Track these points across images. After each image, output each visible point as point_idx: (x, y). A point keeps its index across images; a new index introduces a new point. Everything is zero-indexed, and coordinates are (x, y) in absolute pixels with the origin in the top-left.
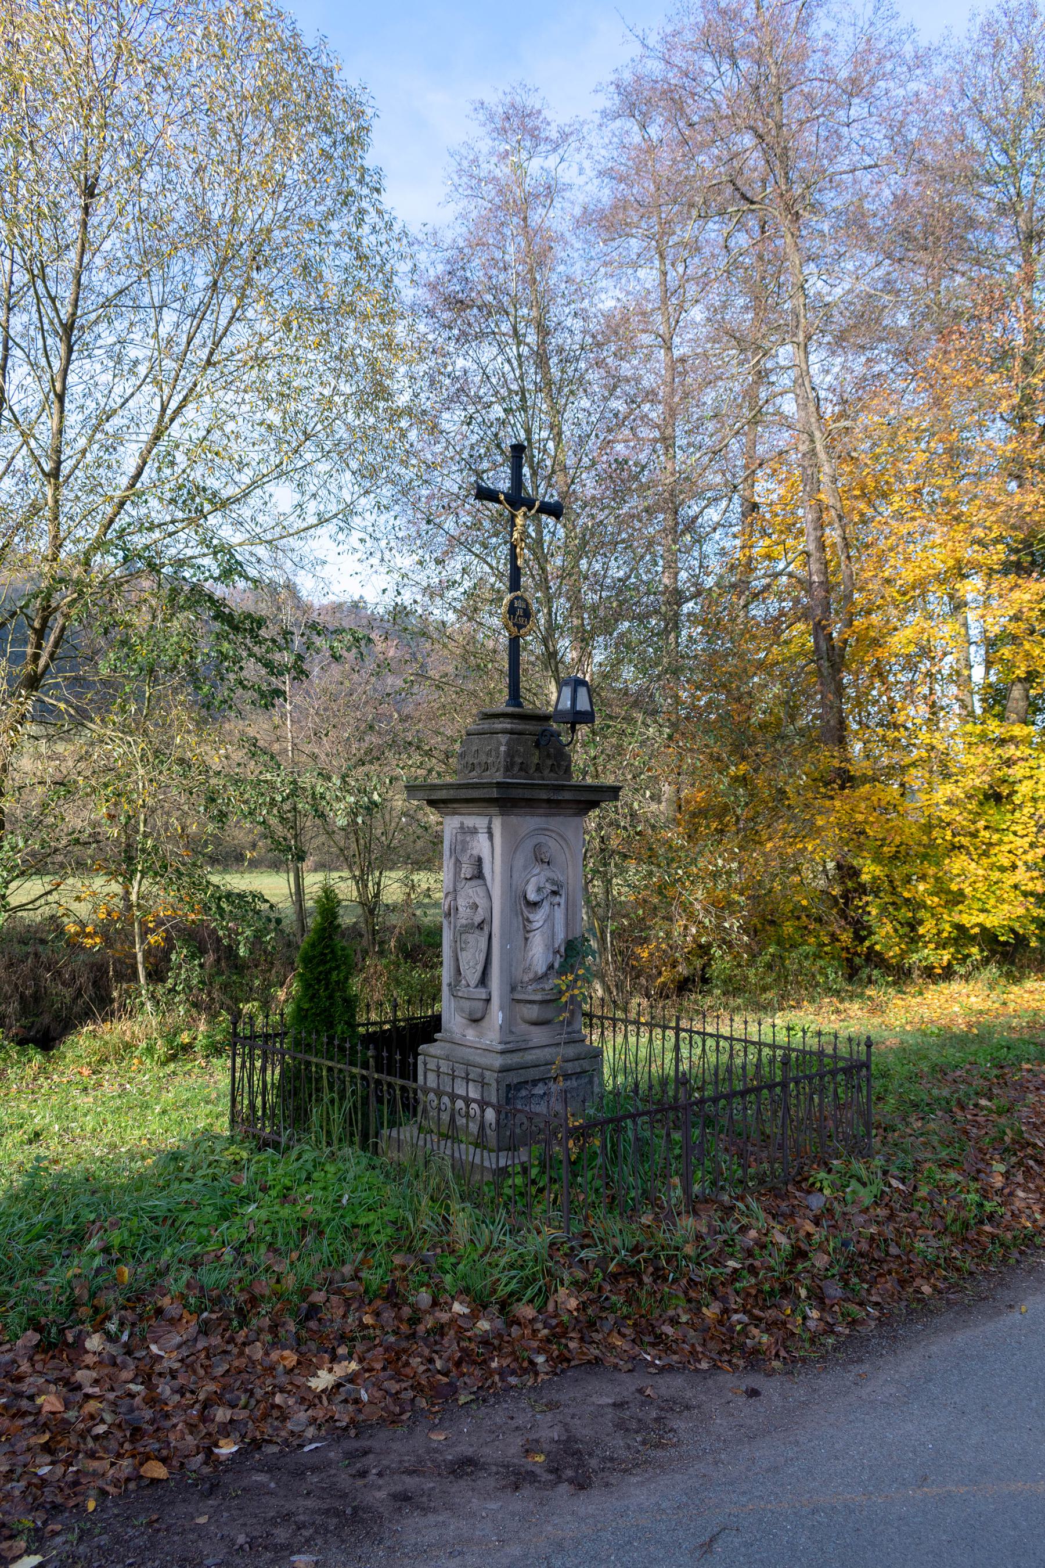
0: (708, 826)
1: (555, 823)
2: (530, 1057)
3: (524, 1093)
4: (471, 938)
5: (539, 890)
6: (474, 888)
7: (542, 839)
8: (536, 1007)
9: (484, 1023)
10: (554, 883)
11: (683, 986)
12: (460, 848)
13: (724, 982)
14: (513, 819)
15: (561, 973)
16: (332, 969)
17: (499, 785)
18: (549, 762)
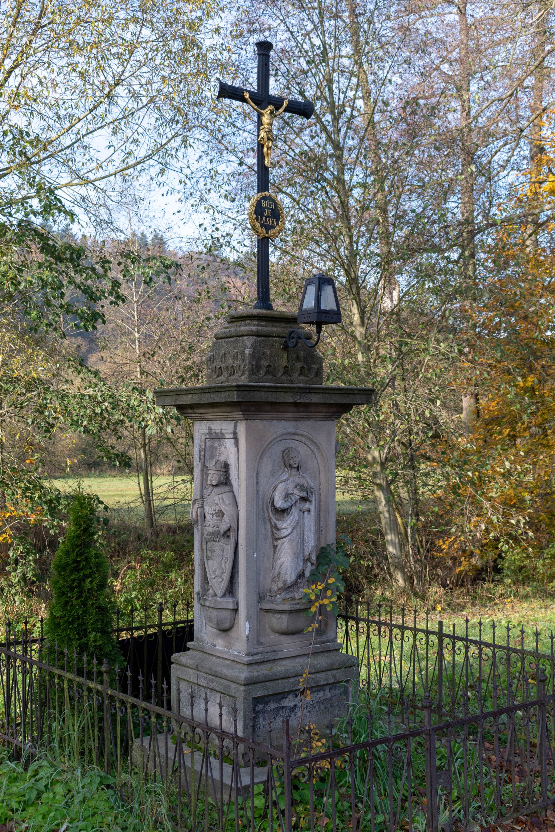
0: (500, 433)
1: (305, 427)
2: (278, 669)
3: (272, 705)
4: (216, 546)
5: (287, 496)
6: (218, 493)
7: (291, 444)
8: (285, 617)
9: (233, 633)
10: (302, 488)
11: (479, 576)
12: (209, 453)
13: (514, 572)
14: (259, 424)
15: (313, 581)
16: (85, 577)
17: (239, 388)
18: (299, 365)
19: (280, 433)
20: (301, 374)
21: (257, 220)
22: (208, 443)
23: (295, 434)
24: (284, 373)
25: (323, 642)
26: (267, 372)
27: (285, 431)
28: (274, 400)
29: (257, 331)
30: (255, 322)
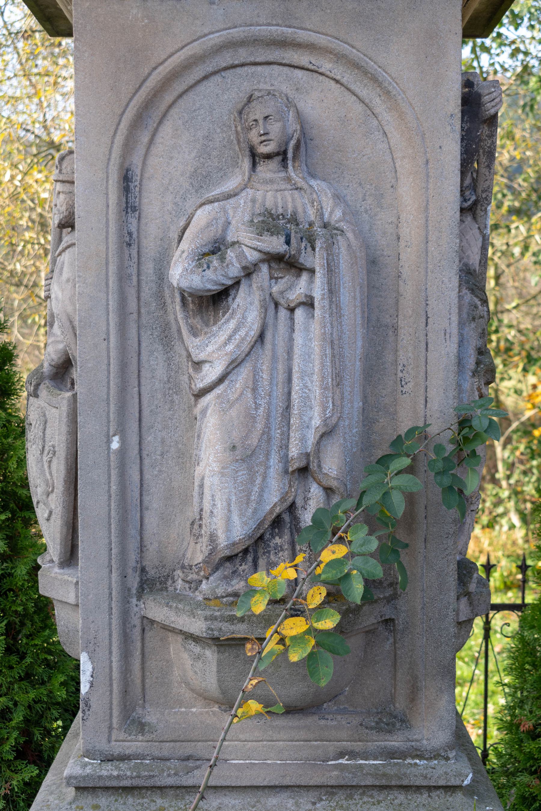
23: (283, 43)
25: (391, 754)
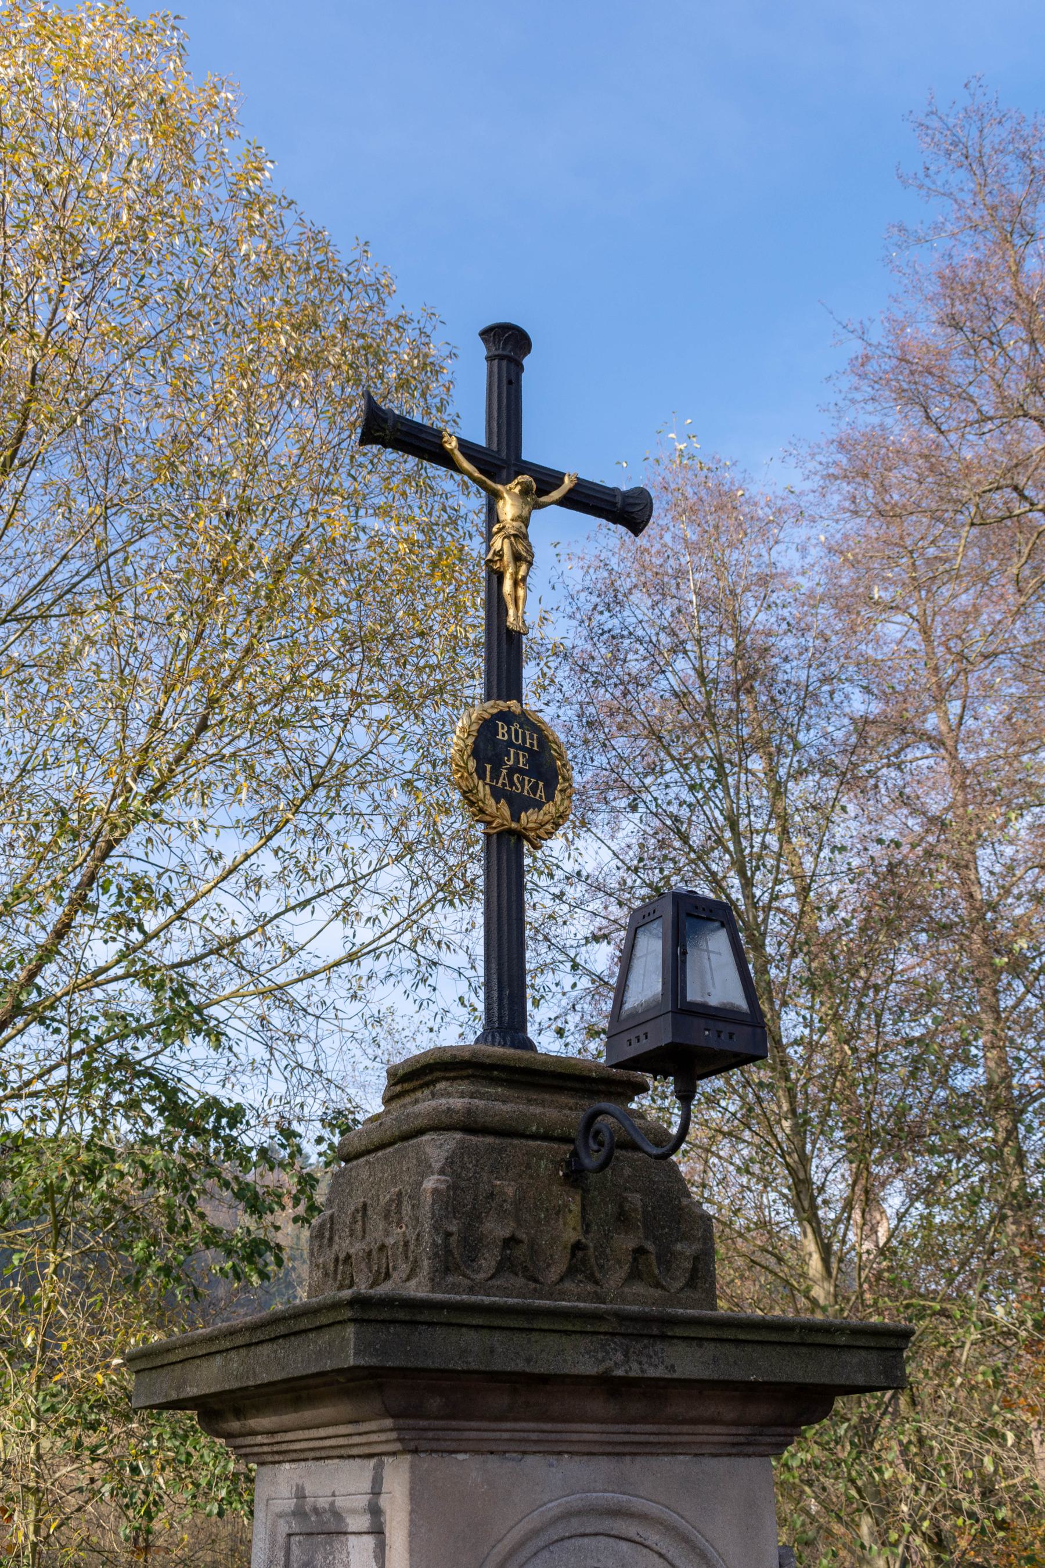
1: (653, 1483)
14: (468, 1470)
18: (626, 1242)
19: (554, 1507)
20: (635, 1275)
21: (482, 776)
22: (295, 1551)
24: (571, 1271)
26: (506, 1265)
27: (575, 1500)
28: (520, 1366)
29: (469, 1112)
30: (464, 1086)
